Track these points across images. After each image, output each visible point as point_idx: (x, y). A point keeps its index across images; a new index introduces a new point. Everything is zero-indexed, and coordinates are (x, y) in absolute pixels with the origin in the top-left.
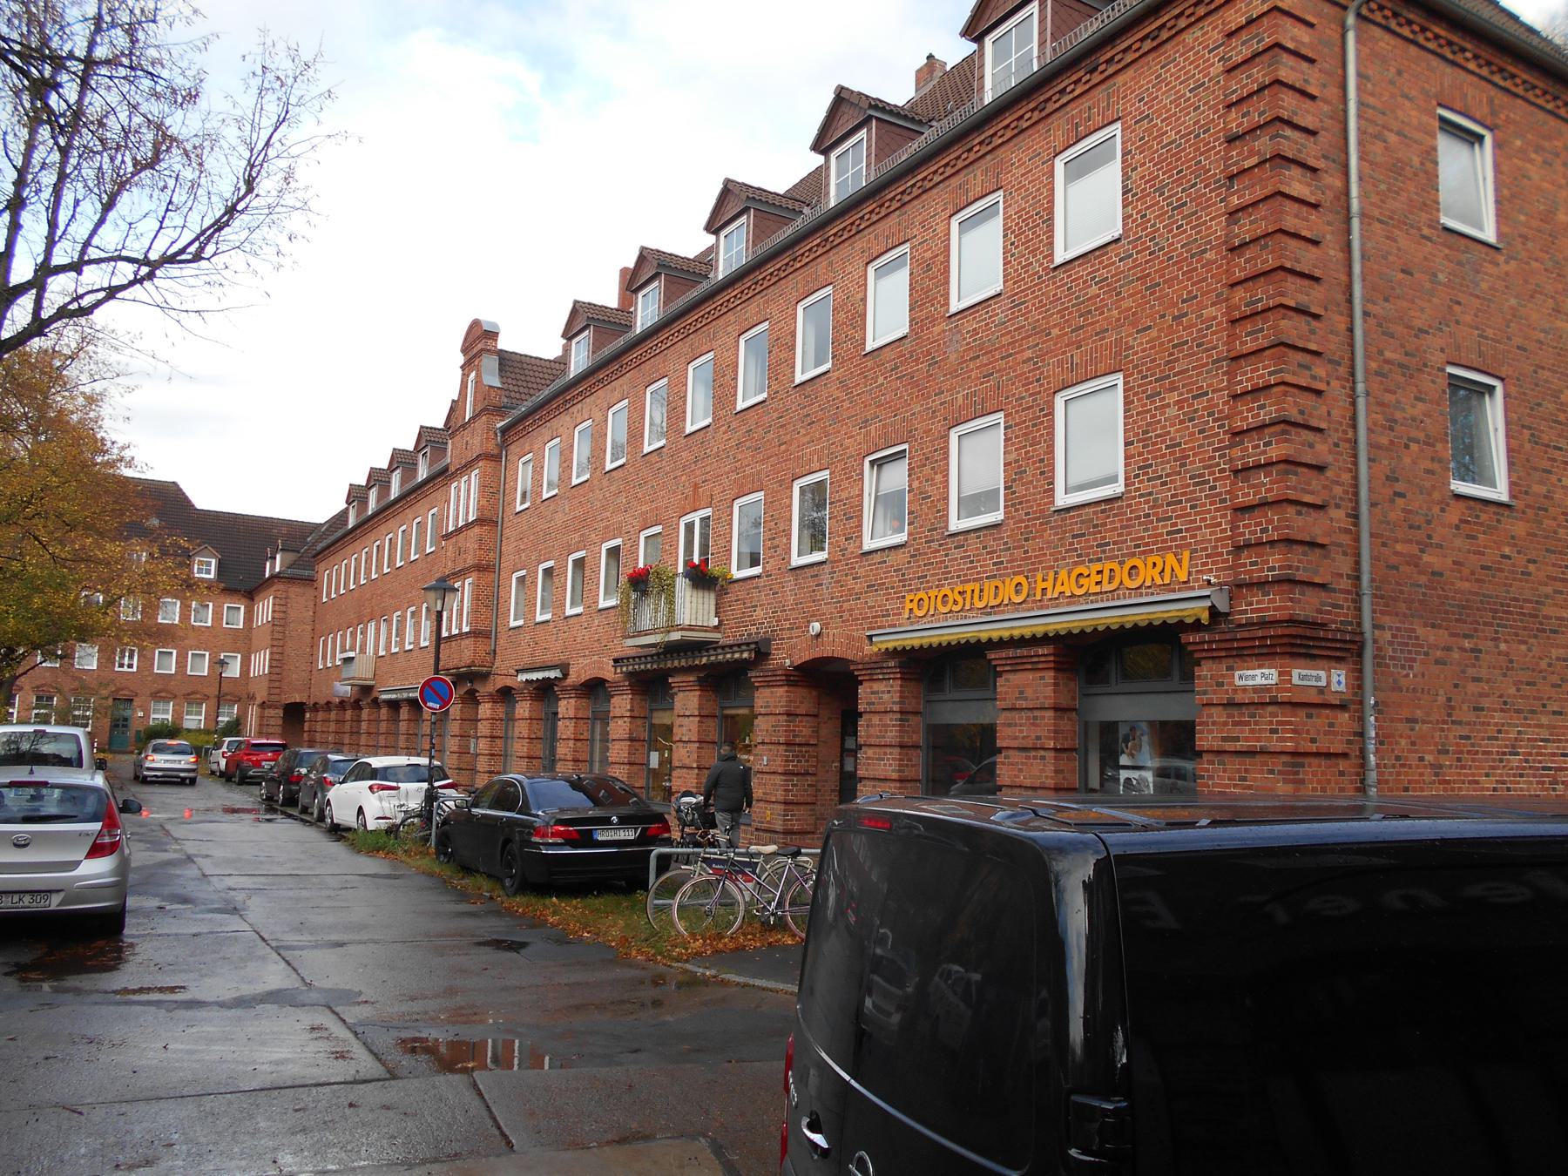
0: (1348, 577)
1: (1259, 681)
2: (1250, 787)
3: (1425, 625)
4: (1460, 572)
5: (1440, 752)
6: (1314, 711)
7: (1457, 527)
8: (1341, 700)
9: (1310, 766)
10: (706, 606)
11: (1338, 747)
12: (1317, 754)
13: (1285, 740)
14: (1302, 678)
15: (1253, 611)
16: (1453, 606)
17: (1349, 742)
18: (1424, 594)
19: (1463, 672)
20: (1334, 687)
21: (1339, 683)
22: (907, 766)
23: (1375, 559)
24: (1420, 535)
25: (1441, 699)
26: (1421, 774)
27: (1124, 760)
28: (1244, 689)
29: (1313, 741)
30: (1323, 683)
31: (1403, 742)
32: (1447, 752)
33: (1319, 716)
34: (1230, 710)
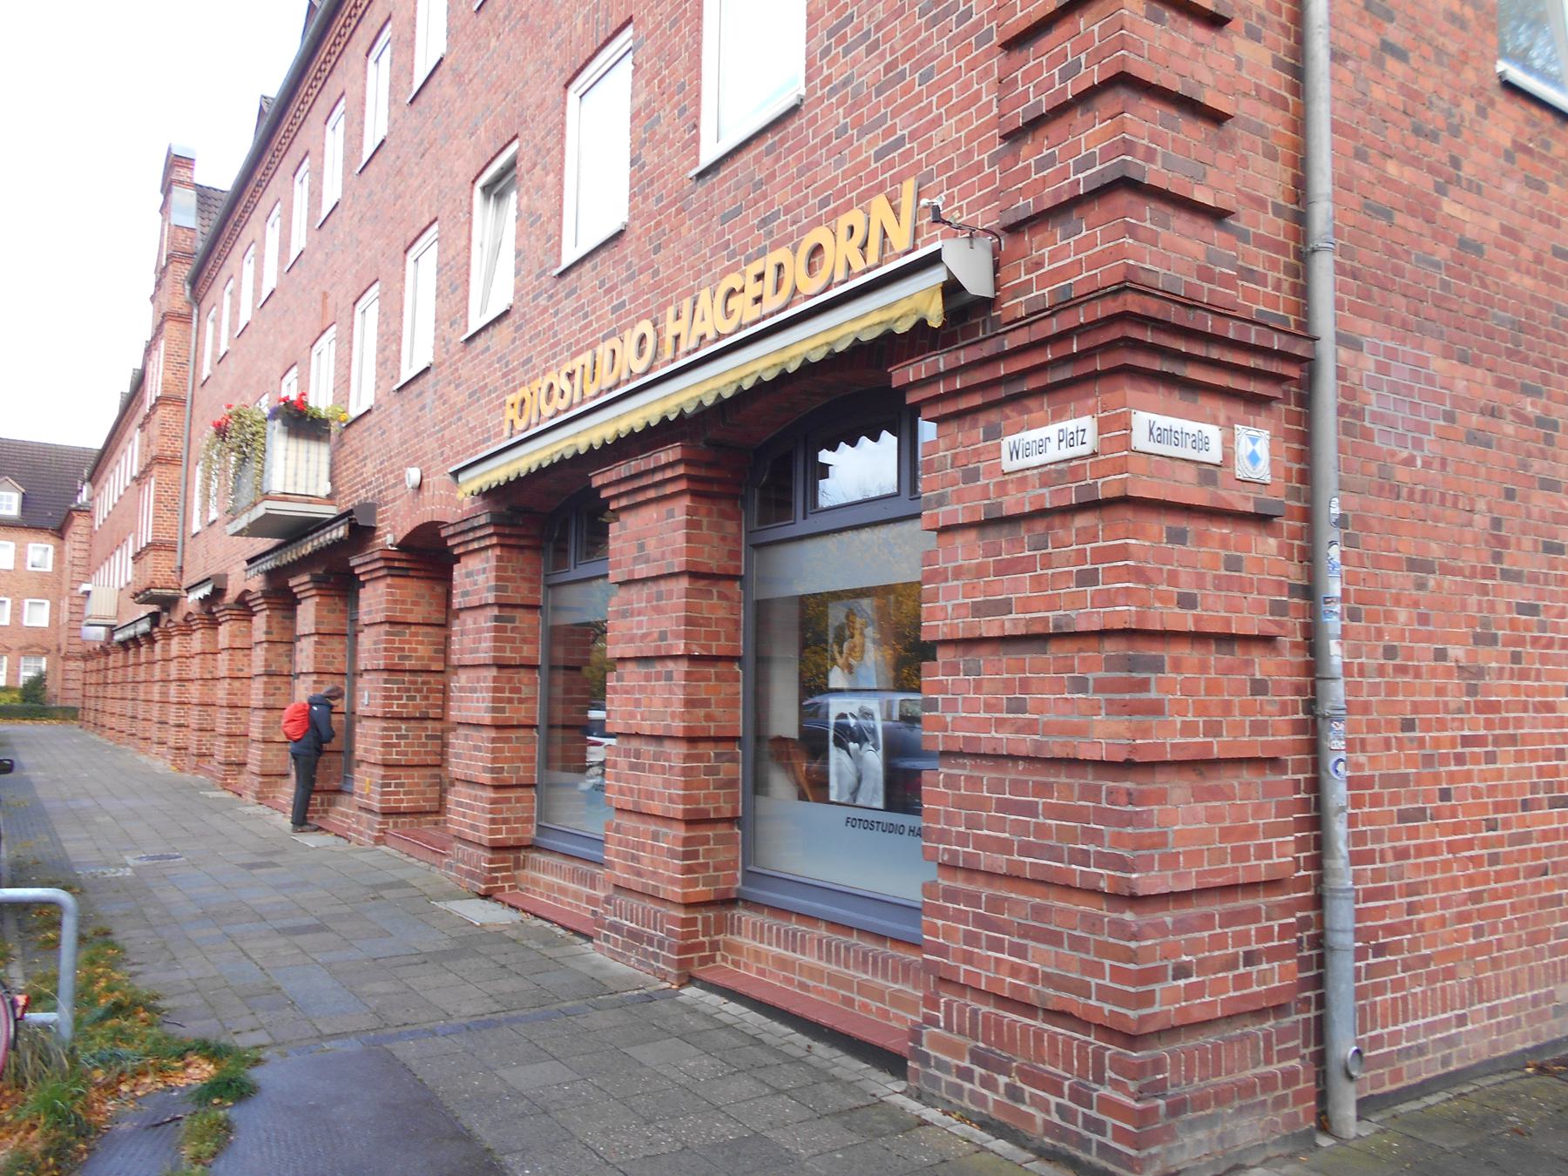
0: (1278, 211)
1: (1054, 453)
2: (1030, 727)
3: (1447, 355)
4: (1515, 251)
5: (1478, 640)
6: (1191, 526)
7: (1509, 157)
8: (1257, 502)
9: (1177, 666)
10: (312, 466)
11: (1253, 623)
12: (1198, 637)
13: (1109, 599)
14: (1154, 433)
15: (1044, 281)
16: (1502, 322)
17: (1278, 608)
18: (1445, 285)
19: (1525, 466)
20: (1243, 469)
21: (1254, 458)
22: (510, 700)
23: (1342, 183)
24: (1438, 153)
25: (1481, 521)
26: (1440, 691)
27: (837, 679)
28: (1021, 478)
29: (1187, 601)
30: (1214, 455)
31: (1402, 614)
32: (1493, 640)
33: (1201, 540)
34: (992, 535)
